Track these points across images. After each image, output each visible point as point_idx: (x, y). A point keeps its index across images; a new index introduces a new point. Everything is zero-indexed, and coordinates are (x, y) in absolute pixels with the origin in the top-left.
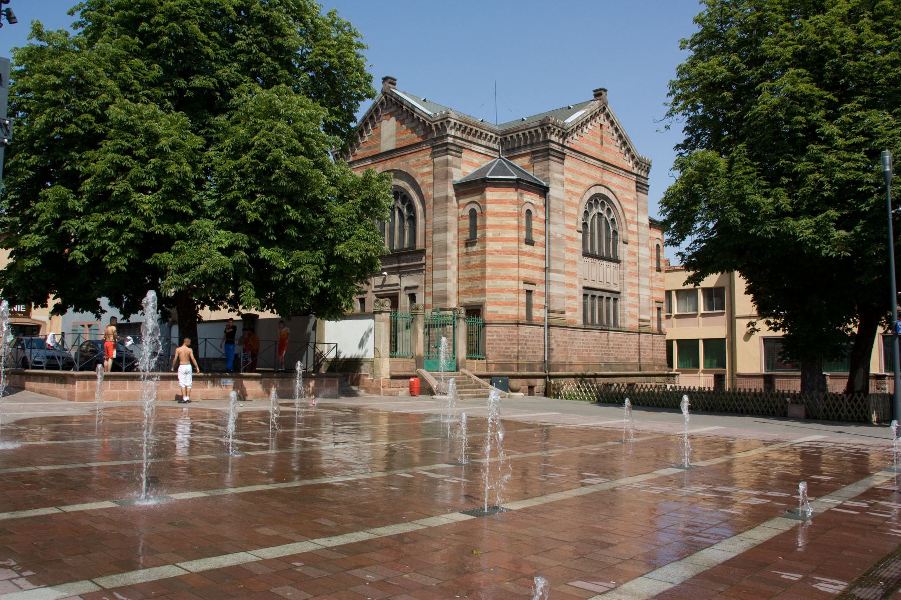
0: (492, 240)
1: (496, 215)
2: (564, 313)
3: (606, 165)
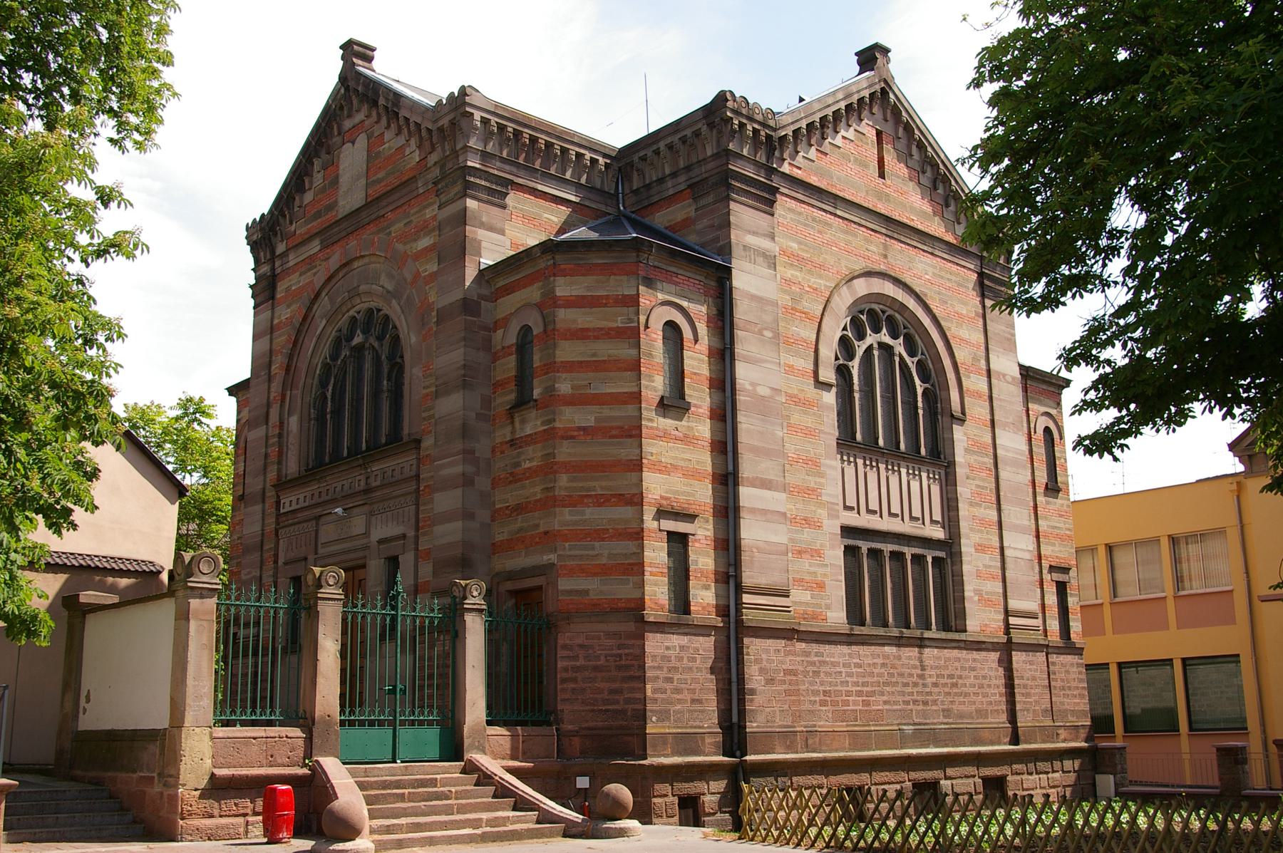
0: (573, 401)
1: (582, 334)
3: (894, 227)
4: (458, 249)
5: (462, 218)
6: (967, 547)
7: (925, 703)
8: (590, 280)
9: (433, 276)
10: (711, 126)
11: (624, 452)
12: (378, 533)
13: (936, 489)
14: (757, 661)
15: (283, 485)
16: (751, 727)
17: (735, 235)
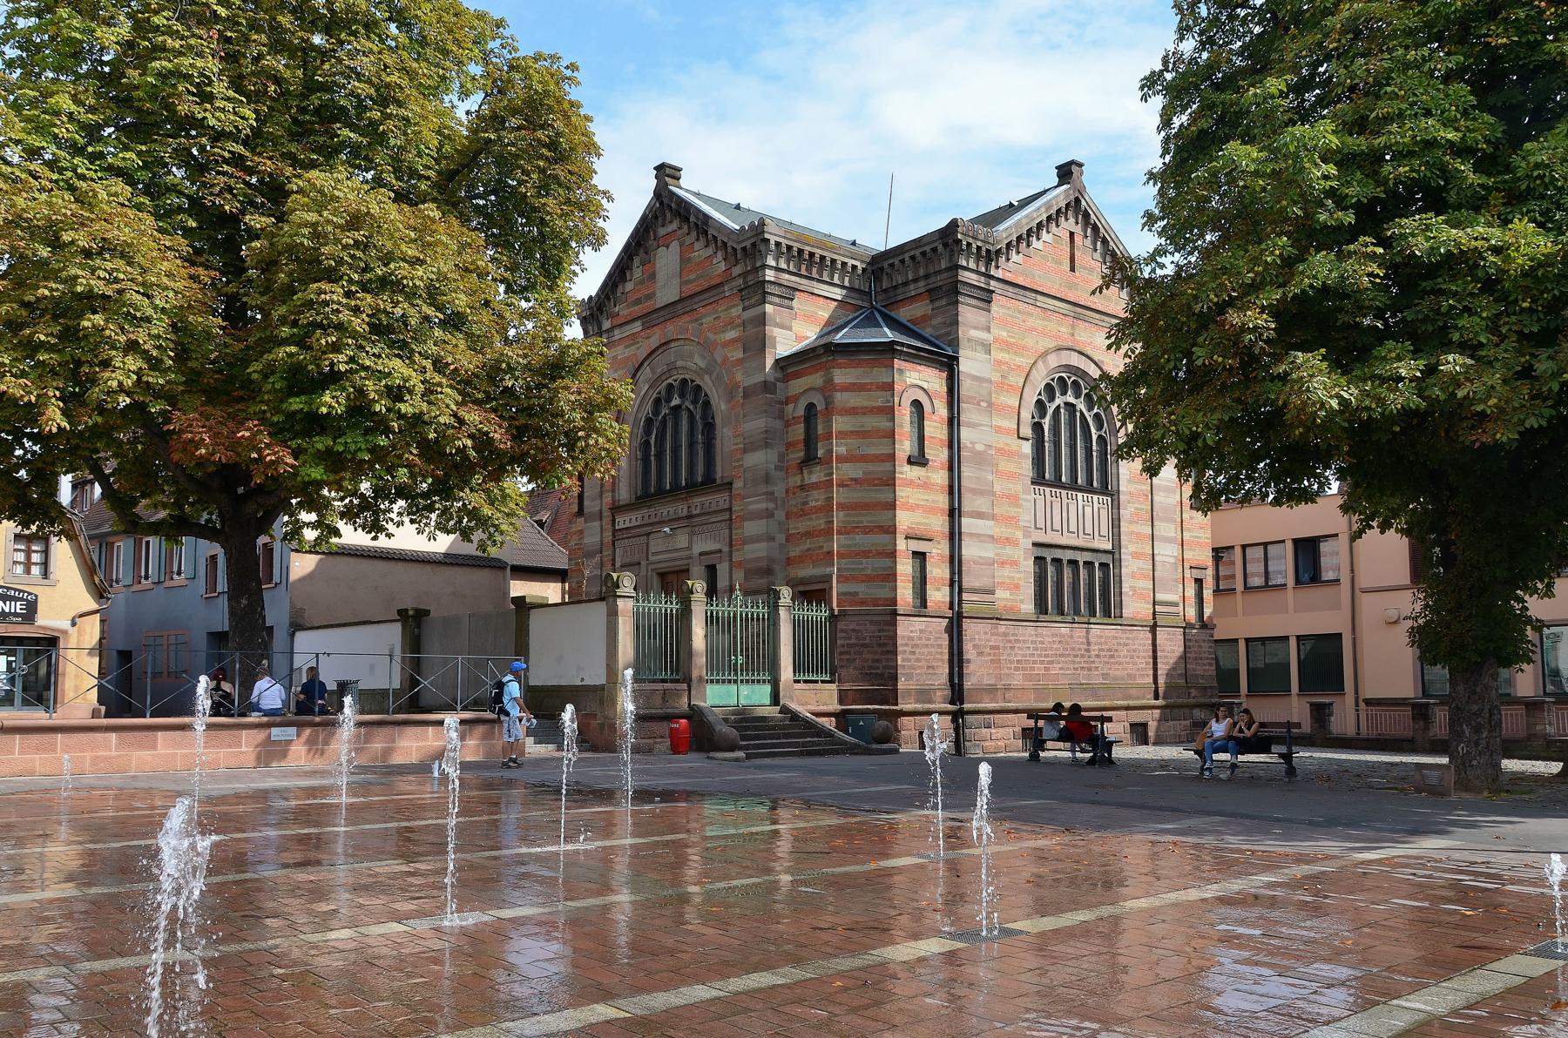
2: (992, 593)
4: (757, 343)
5: (762, 320)
6: (1128, 548)
7: (1089, 669)
8: (859, 371)
9: (740, 361)
10: (945, 245)
11: (882, 496)
12: (698, 548)
13: (1104, 513)
14: (972, 639)
15: (616, 509)
16: (967, 684)
17: (962, 331)
